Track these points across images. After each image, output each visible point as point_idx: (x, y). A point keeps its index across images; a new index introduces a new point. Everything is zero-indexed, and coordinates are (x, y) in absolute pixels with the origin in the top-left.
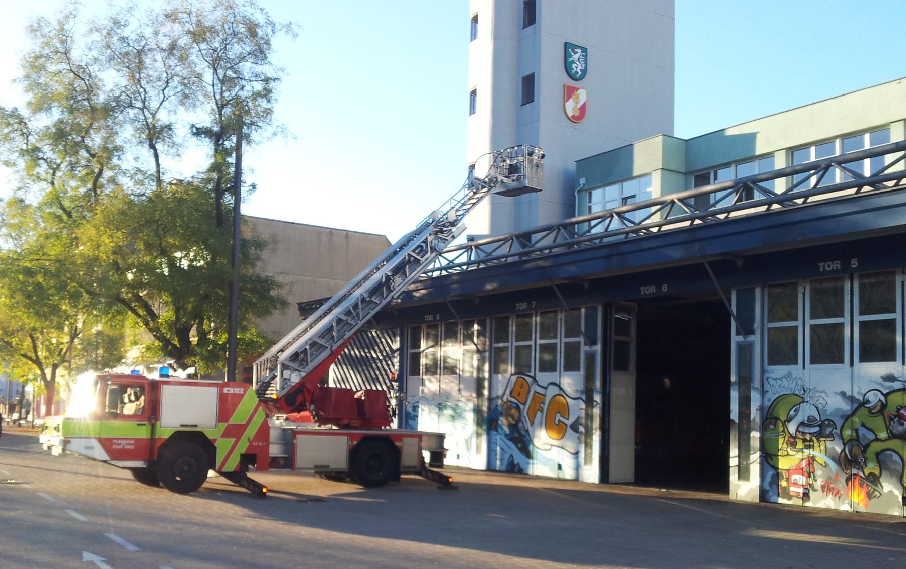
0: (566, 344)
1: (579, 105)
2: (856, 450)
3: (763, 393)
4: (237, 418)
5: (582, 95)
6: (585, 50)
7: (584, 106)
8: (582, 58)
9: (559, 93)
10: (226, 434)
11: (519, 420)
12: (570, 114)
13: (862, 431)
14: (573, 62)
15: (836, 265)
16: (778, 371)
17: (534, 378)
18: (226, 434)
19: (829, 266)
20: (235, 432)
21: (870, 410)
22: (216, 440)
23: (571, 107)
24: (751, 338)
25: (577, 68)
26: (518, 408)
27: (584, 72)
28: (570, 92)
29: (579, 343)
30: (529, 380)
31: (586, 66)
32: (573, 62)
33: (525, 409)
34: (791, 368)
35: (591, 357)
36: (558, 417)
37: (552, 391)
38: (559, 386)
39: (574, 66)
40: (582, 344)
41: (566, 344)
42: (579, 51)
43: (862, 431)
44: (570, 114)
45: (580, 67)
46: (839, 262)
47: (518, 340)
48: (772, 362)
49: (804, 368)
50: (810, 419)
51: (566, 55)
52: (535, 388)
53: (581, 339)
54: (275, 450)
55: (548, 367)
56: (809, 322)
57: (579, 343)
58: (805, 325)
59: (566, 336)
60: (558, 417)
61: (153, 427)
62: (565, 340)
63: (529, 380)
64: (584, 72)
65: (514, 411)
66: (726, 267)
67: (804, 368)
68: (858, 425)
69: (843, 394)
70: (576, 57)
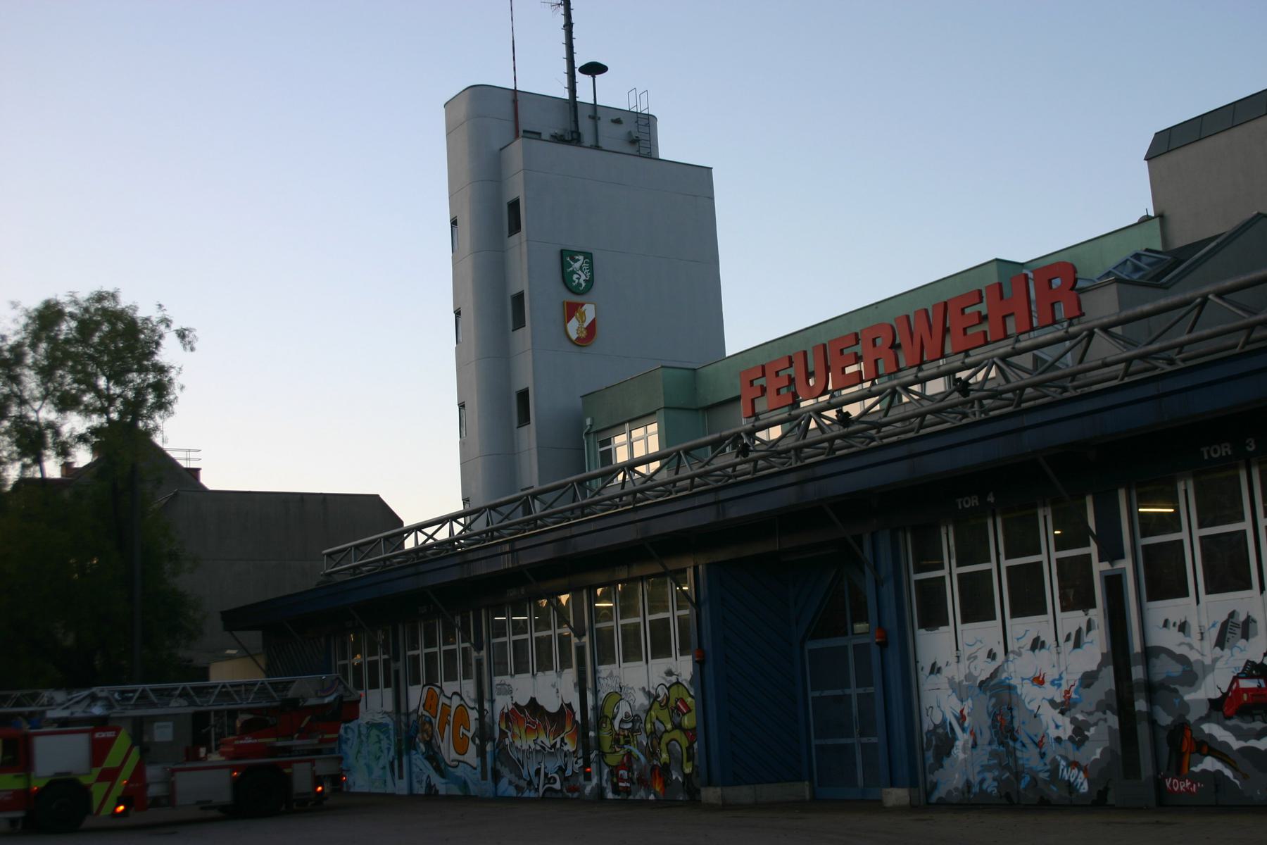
0: (960, 576)
1: (586, 325)
2: (655, 742)
3: (596, 693)
4: (112, 760)
5: (589, 312)
6: (588, 256)
7: (593, 323)
8: (586, 267)
9: (557, 312)
10: (100, 779)
11: (432, 737)
12: (574, 336)
13: (658, 724)
14: (574, 272)
15: (1225, 450)
16: (604, 670)
17: (441, 688)
18: (100, 779)
19: (1215, 451)
20: (110, 776)
21: (660, 703)
22: (90, 785)
23: (574, 328)
24: (1120, 564)
25: (580, 278)
26: (431, 723)
27: (590, 282)
28: (572, 310)
29: (1089, 556)
30: (437, 690)
31: (592, 275)
32: (574, 272)
33: (436, 722)
34: (612, 666)
35: (581, 649)
36: (462, 730)
37: (456, 701)
38: (460, 696)
39: (575, 277)
40: (1095, 558)
41: (960, 576)
42: (581, 258)
43: (658, 724)
44: (574, 336)
45: (583, 277)
46: (1228, 444)
47: (426, 647)
48: (1153, 597)
49: (1198, 602)
50: (627, 715)
51: (564, 265)
52: (443, 700)
53: (1093, 549)
54: (154, 791)
55: (451, 676)
56: (1198, 533)
57: (1089, 556)
58: (998, 566)
59: (959, 564)
60: (462, 730)
61: (29, 779)
62: (957, 571)
63: (437, 690)
64: (590, 282)
65: (427, 726)
66: (856, 507)
67: (1198, 602)
68: (654, 719)
69: (644, 689)
70: (577, 265)
